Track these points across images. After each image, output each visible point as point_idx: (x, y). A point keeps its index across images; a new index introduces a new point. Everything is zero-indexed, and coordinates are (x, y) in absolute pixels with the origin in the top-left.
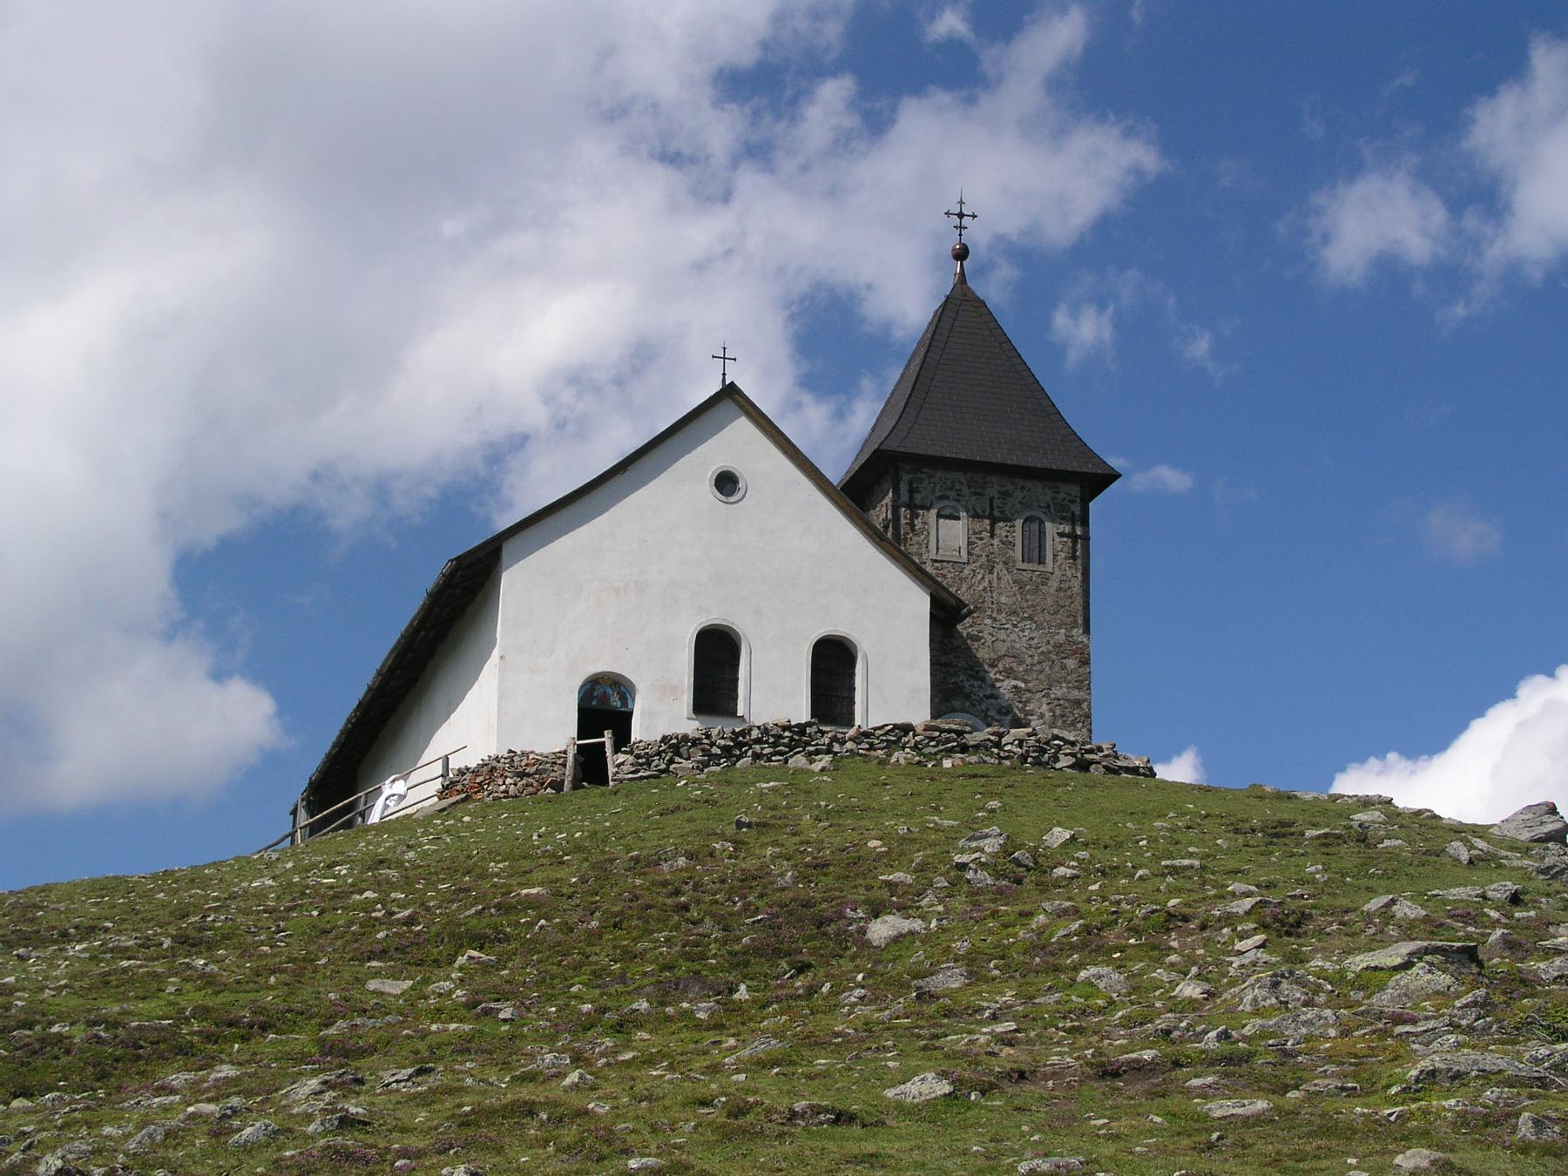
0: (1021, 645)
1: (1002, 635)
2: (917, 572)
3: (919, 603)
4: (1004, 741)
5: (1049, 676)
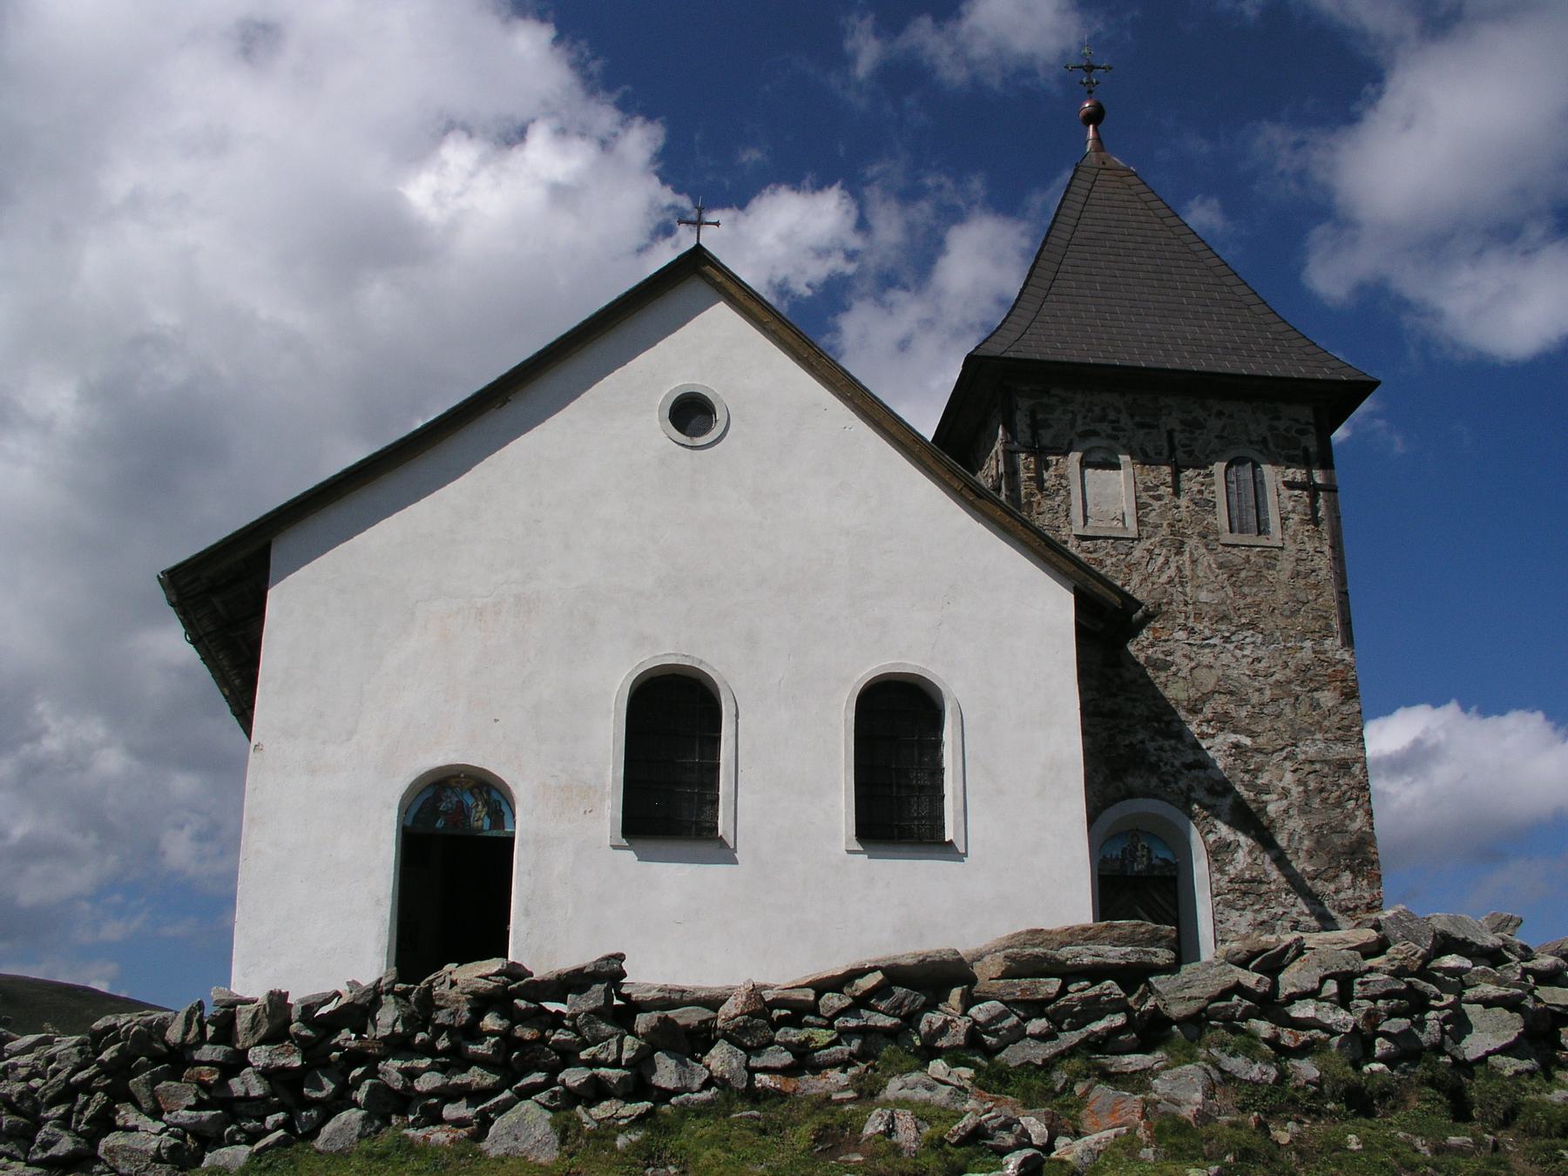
0: (1240, 672)
1: (1206, 657)
2: (1048, 552)
3: (1053, 608)
4: (1291, 980)
5: (1291, 723)
